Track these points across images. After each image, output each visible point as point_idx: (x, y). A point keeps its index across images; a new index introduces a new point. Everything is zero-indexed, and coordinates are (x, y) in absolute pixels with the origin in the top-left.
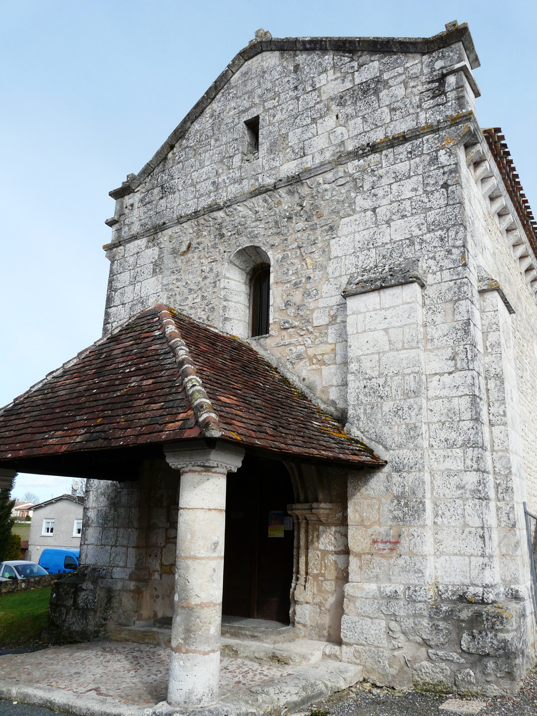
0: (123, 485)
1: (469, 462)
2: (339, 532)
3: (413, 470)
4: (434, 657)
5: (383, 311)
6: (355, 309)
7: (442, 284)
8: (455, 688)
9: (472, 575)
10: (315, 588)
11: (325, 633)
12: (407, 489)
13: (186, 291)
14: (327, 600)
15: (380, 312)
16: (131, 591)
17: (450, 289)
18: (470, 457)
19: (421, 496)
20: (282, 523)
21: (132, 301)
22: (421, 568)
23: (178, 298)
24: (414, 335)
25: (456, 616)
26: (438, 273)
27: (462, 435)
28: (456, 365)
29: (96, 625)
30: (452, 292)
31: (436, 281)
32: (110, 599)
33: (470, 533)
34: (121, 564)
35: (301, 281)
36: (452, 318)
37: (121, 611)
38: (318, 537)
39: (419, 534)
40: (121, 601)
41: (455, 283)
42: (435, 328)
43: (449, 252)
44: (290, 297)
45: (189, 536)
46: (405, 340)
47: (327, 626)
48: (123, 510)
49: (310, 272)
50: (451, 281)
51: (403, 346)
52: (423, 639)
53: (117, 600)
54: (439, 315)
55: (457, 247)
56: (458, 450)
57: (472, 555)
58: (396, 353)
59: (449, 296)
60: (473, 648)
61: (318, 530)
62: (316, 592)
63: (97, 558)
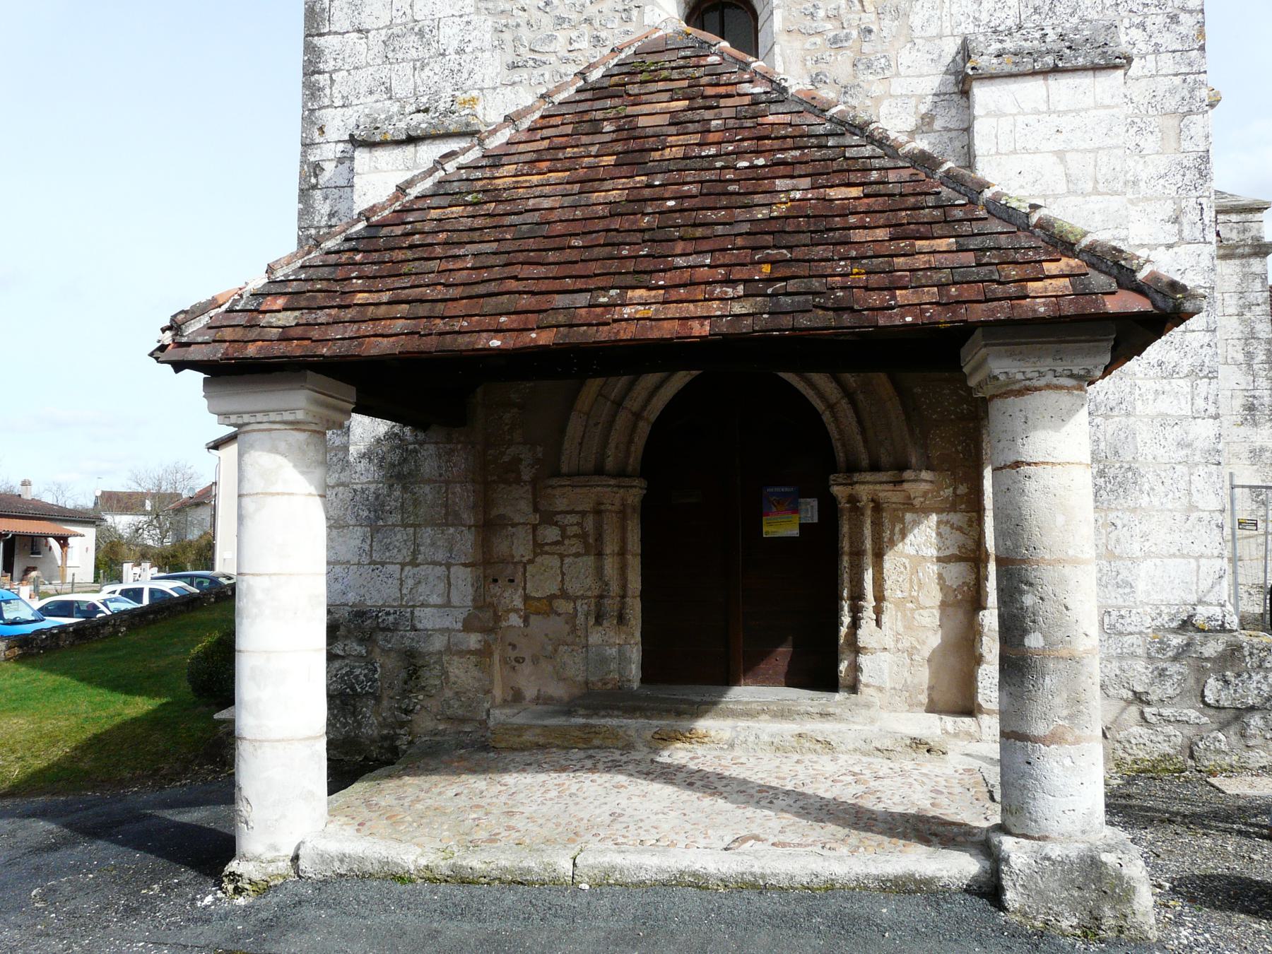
0: (421, 436)
1: (1200, 403)
2: (948, 522)
3: (1116, 412)
4: (1153, 720)
5: (1054, 116)
6: (992, 107)
7: (1159, 79)
8: (1190, 762)
9: (1201, 587)
10: (899, 624)
11: (924, 699)
12: (1102, 445)
13: (547, 21)
14: (924, 643)
15: (1048, 119)
16: (470, 652)
17: (1172, 91)
18: (1203, 395)
19: (1129, 458)
20: (795, 511)
21: (389, 27)
22: (1130, 579)
23: (524, 33)
24: (1118, 169)
25: (1196, 652)
26: (1151, 58)
27: (1189, 356)
28: (1180, 231)
29: (382, 725)
30: (1178, 98)
31: (1146, 72)
32: (415, 671)
33: (1200, 520)
34: (435, 599)
35: (847, 37)
36: (1175, 146)
37: (448, 693)
38: (904, 535)
39: (1125, 522)
40: (445, 673)
41: (1184, 81)
42: (1142, 161)
43: (1174, 19)
44: (822, 66)
45: (1060, 520)
46: (1099, 177)
47: (925, 686)
48: (427, 489)
49: (869, 19)
50: (1176, 75)
51: (1095, 188)
52: (1135, 693)
53: (436, 672)
54: (1151, 138)
55: (1191, 12)
56: (1181, 382)
57: (1201, 556)
58: (1080, 199)
59: (1171, 103)
60: (1227, 700)
61: (902, 520)
62: (901, 630)
63: (362, 591)
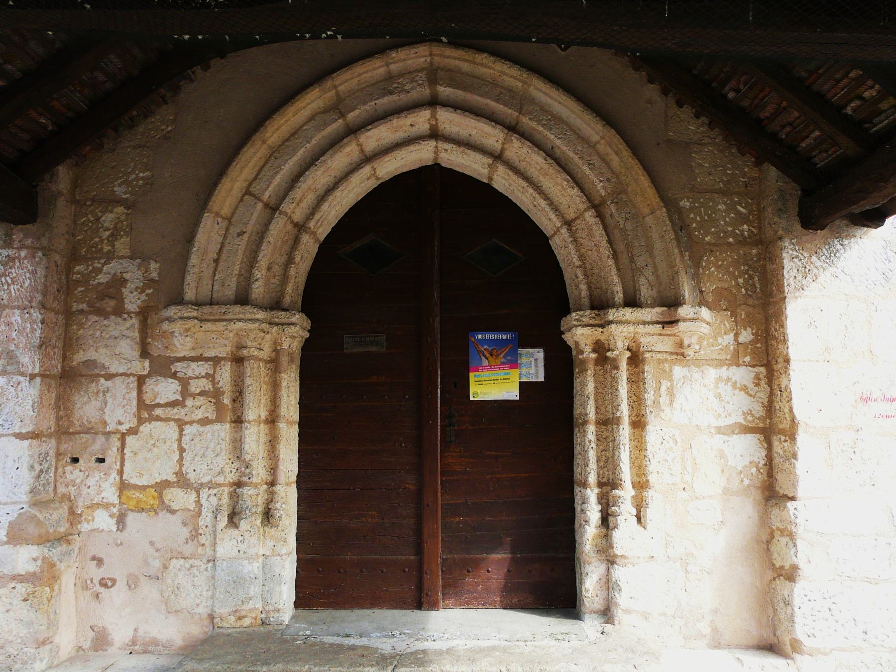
2: (728, 379)
11: (705, 628)
20: (514, 365)
61: (669, 376)
